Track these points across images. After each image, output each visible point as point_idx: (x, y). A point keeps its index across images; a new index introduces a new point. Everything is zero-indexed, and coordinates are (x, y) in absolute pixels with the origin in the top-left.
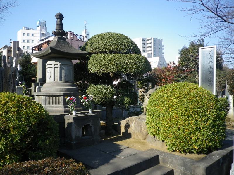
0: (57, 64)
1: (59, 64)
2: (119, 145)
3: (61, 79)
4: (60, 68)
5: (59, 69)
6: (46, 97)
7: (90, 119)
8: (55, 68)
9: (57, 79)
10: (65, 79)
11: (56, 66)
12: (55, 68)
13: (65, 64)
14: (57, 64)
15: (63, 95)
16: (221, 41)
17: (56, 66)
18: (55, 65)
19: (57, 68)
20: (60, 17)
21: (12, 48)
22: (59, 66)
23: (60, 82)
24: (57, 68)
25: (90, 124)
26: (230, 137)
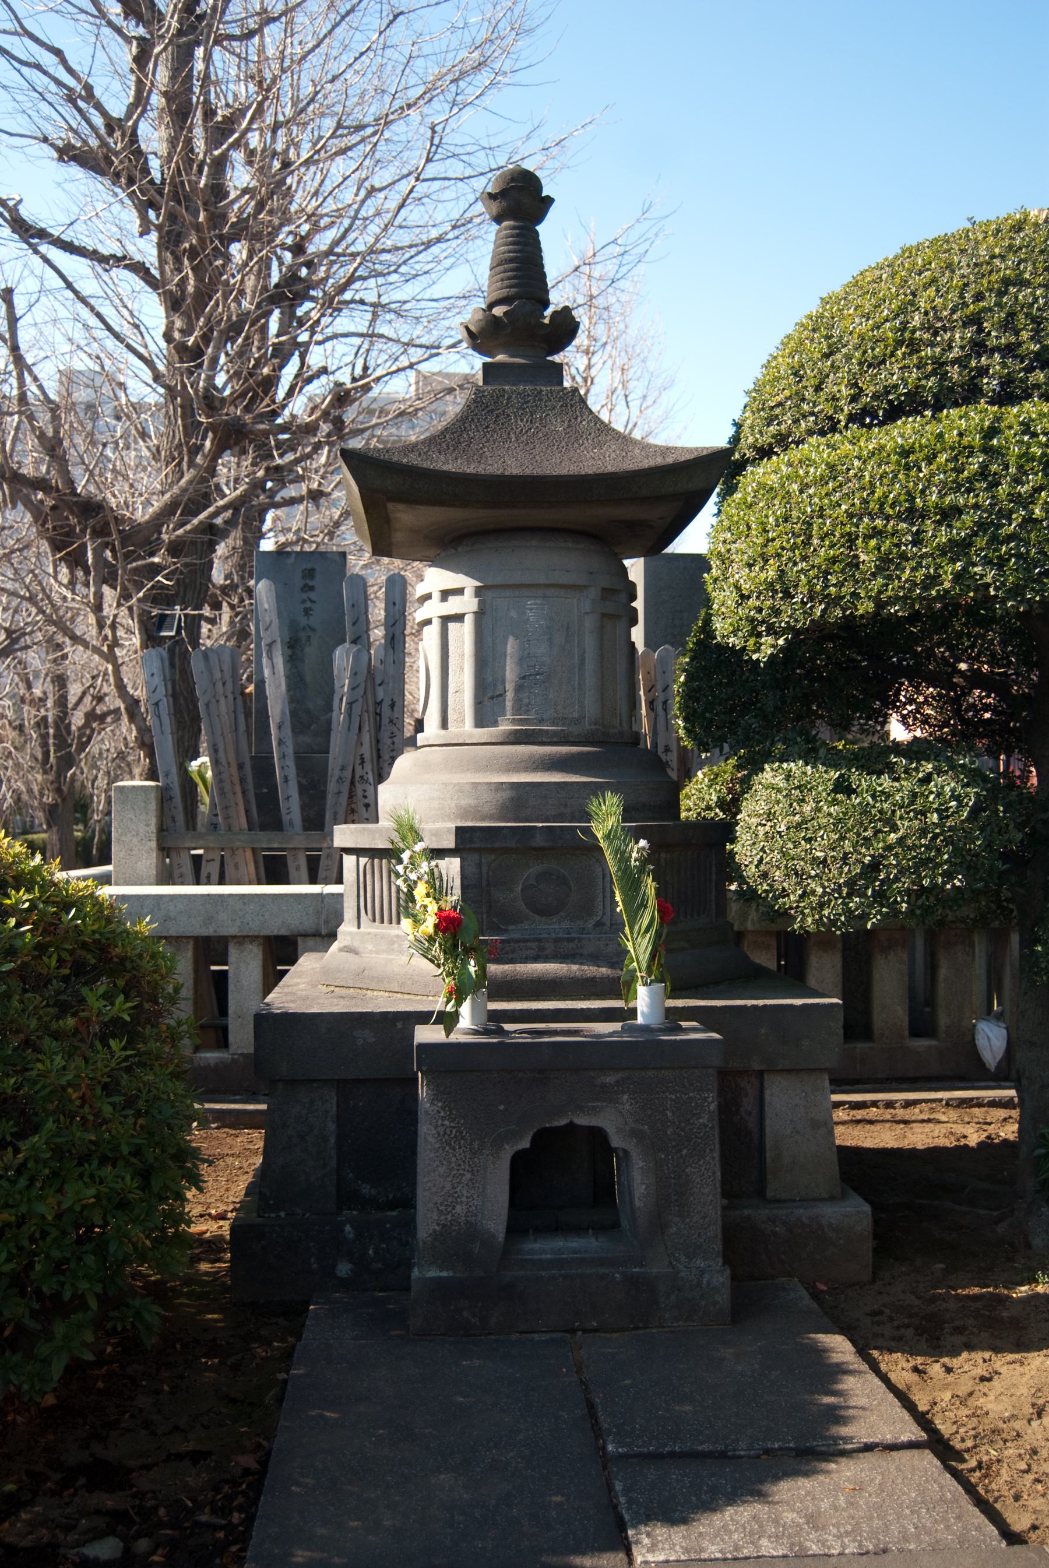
0: (460, 591)
1: (469, 584)
2: (826, 1350)
3: (486, 708)
4: (480, 615)
5: (469, 620)
6: (363, 861)
7: (610, 1079)
8: (446, 620)
9: (462, 714)
10: (518, 708)
11: (454, 605)
12: (452, 626)
13: (518, 578)
14: (460, 591)
15: (450, 843)
16: (846, 1118)
17: (454, 605)
18: (445, 594)
19: (459, 618)
20: (521, 201)
21: (634, 598)
22: (467, 603)
23: (484, 734)
24: (459, 618)
25: (611, 1121)
26: (850, 446)
